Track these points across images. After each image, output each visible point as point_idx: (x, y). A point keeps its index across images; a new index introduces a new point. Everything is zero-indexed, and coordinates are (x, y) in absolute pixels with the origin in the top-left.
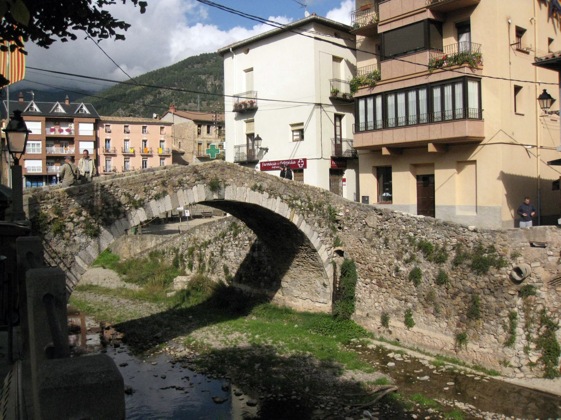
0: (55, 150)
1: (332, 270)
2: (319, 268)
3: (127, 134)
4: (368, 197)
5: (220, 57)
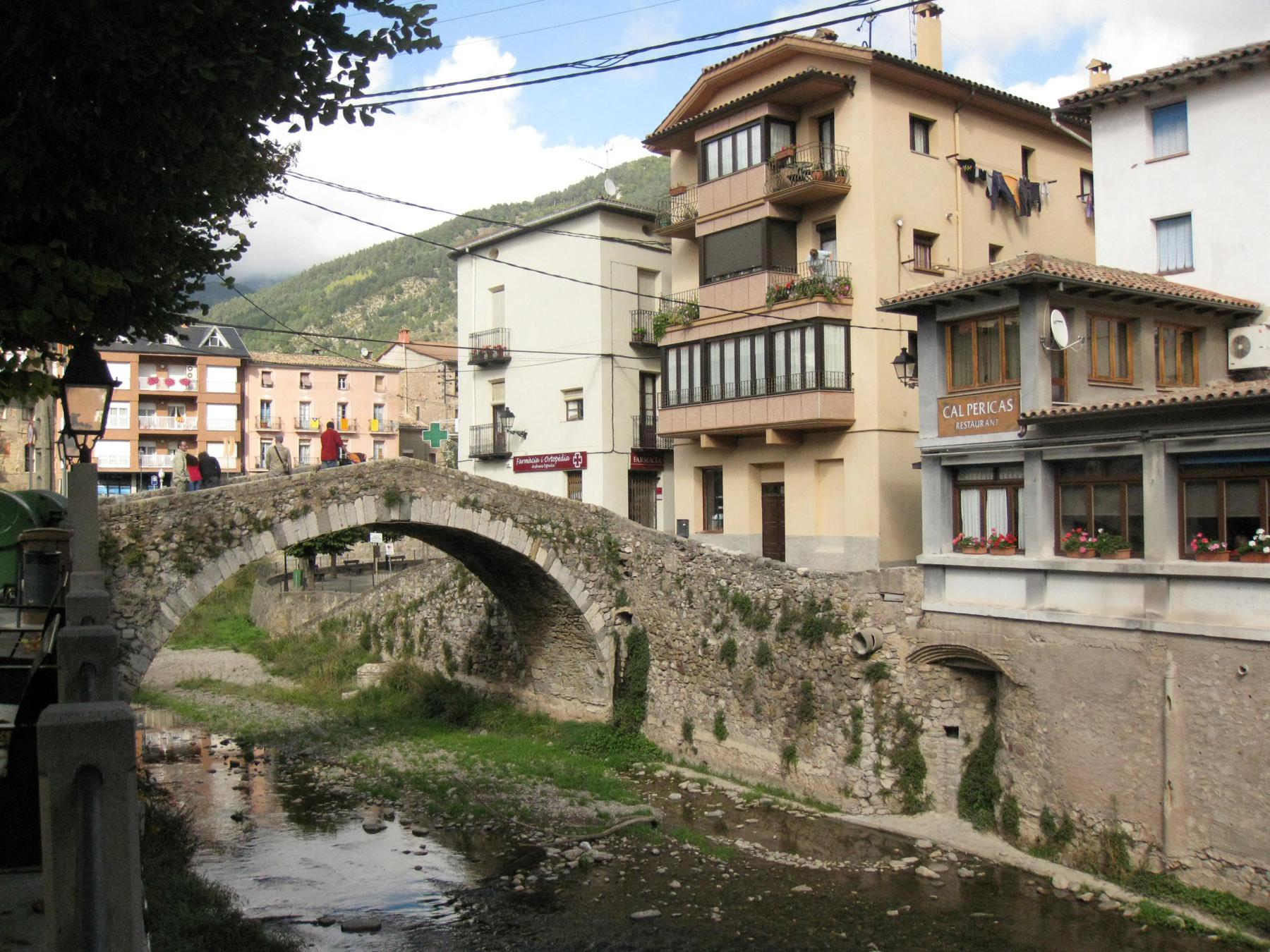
0: (159, 422)
1: (612, 647)
2: (589, 643)
3: (306, 391)
4: (687, 521)
5: (451, 261)
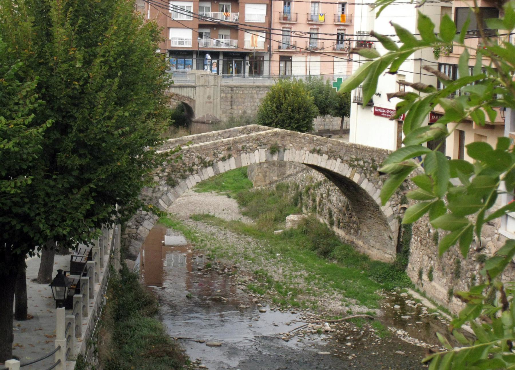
2: (384, 222)
